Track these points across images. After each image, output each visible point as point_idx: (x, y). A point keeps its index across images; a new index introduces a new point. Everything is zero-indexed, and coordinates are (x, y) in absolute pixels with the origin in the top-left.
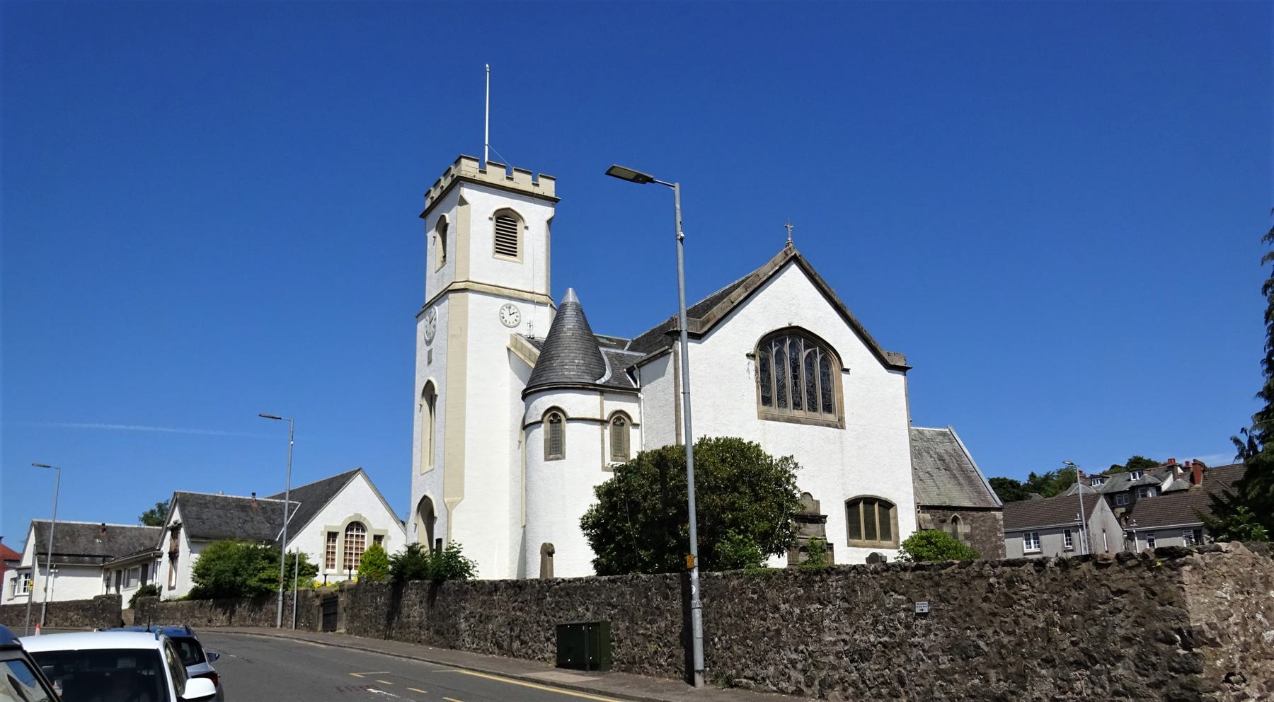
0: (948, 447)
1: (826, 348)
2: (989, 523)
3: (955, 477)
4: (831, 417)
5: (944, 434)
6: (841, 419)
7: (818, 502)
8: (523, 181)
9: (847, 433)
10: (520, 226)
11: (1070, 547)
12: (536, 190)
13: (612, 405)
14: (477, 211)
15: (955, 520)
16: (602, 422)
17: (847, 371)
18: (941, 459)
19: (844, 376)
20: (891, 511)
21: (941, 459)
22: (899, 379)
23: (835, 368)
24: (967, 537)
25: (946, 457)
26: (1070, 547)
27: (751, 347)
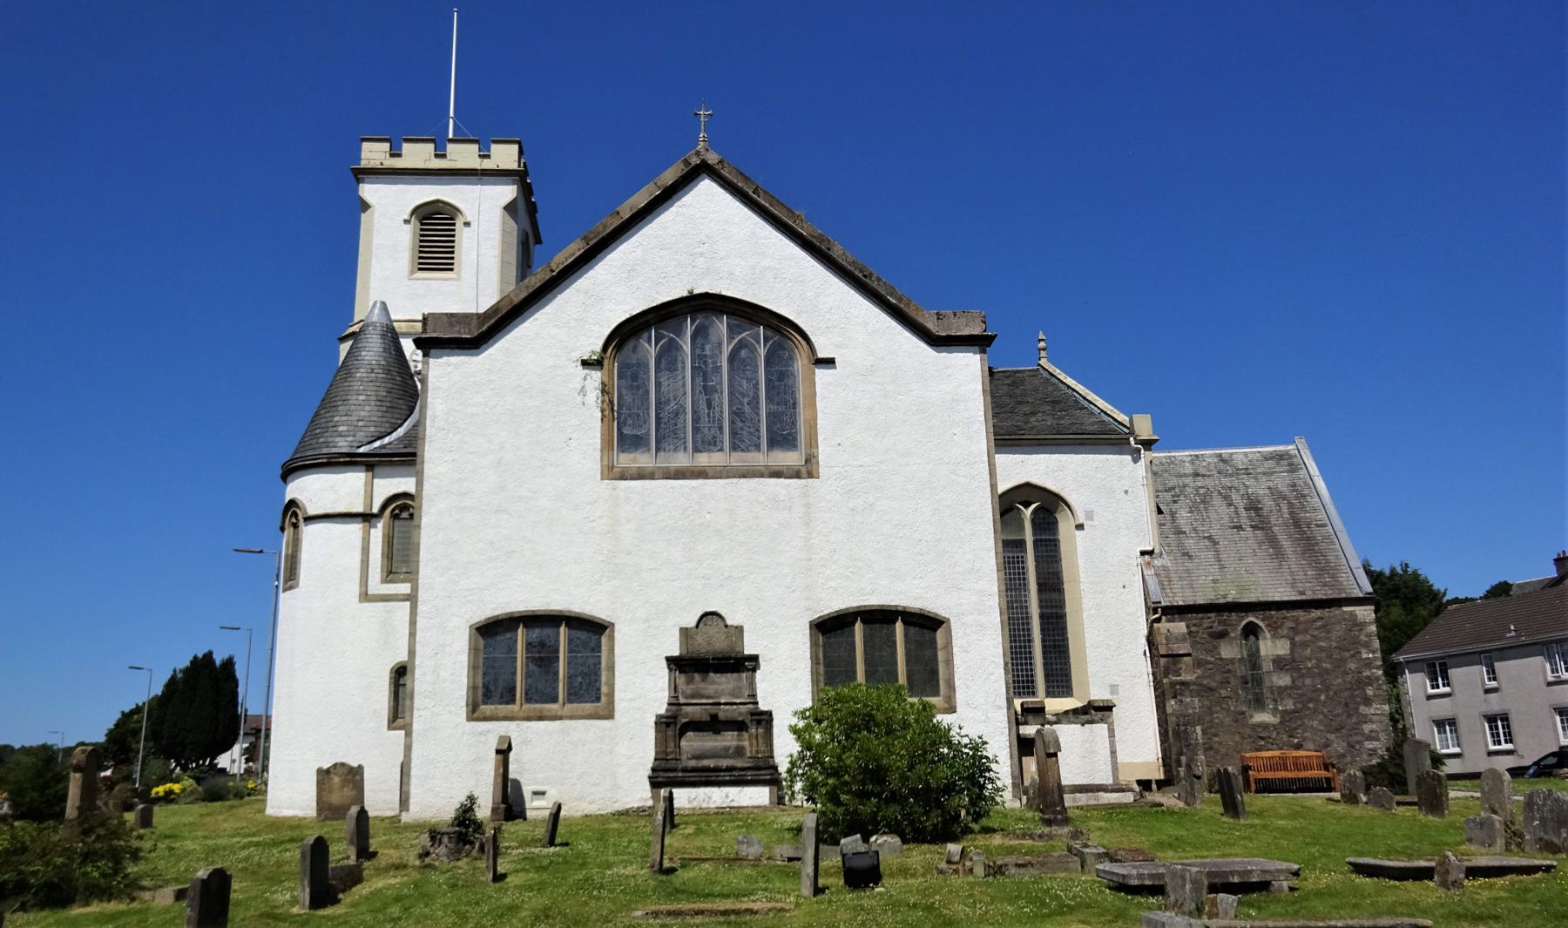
0: (1281, 481)
1: (780, 327)
2: (1338, 631)
3: (1273, 541)
4: (790, 458)
5: (1280, 457)
6: (811, 460)
7: (739, 630)
8: (463, 156)
9: (822, 487)
10: (459, 222)
11: (1494, 684)
12: (487, 164)
13: (389, 485)
14: (388, 211)
15: (1251, 631)
16: (367, 518)
17: (829, 362)
18: (1254, 506)
19: (821, 374)
20: (940, 634)
21: (1254, 506)
22: (969, 364)
23: (801, 364)
24: (1280, 664)
25: (1268, 503)
26: (1494, 684)
27: (593, 344)
